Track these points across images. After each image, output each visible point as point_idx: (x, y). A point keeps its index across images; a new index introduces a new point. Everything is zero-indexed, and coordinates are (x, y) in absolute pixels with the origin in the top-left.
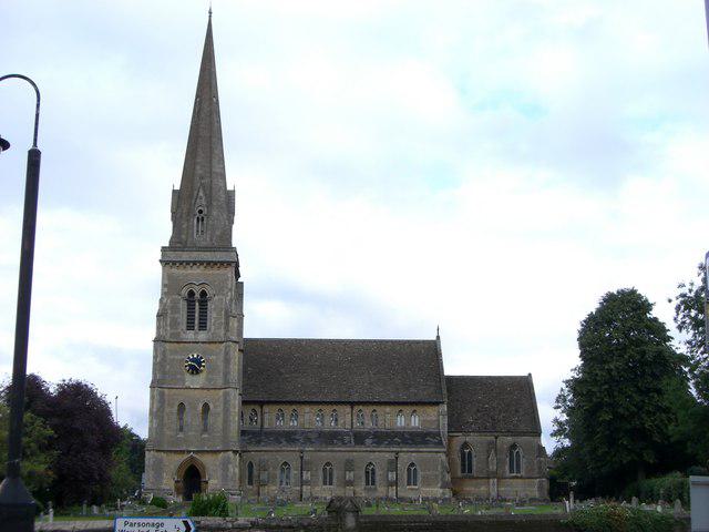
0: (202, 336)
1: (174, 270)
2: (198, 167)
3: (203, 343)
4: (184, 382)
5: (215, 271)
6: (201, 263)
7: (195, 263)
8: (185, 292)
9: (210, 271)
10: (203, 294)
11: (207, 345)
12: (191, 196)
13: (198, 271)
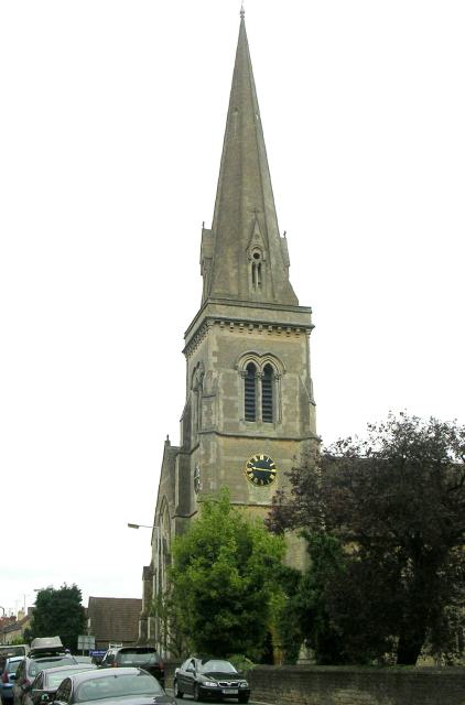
0: (267, 430)
1: (226, 332)
2: (246, 198)
3: (272, 439)
4: (246, 495)
5: (282, 338)
6: (266, 325)
7: (256, 325)
8: (242, 365)
9: (275, 338)
10: (268, 369)
11: (277, 443)
12: (238, 236)
13: (259, 337)
